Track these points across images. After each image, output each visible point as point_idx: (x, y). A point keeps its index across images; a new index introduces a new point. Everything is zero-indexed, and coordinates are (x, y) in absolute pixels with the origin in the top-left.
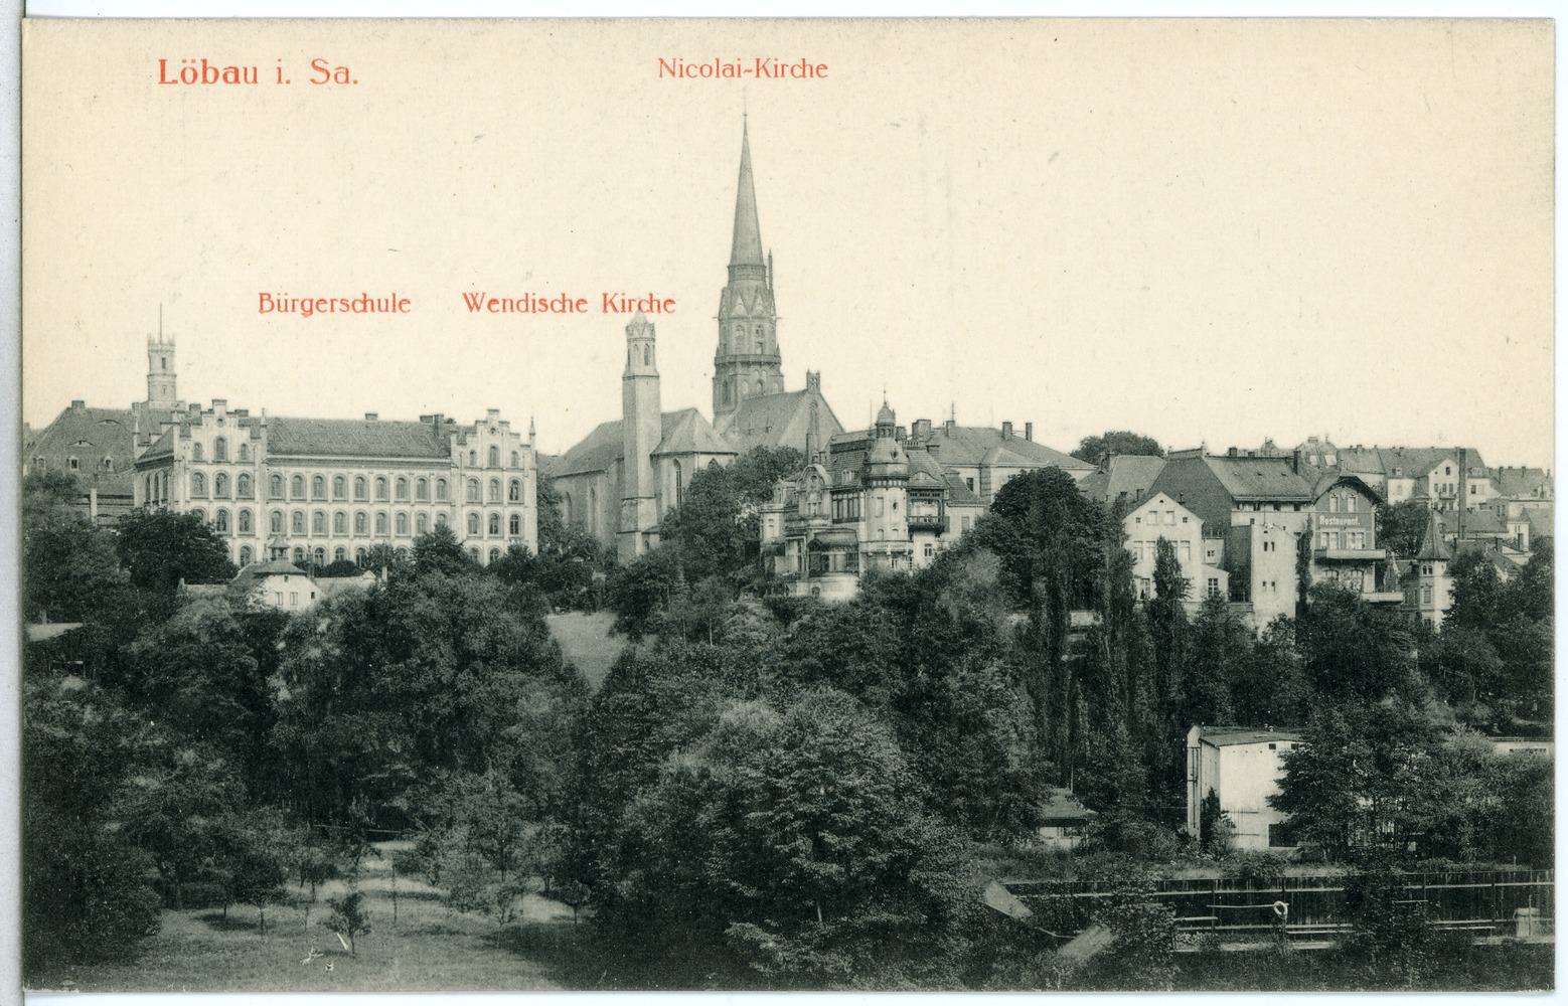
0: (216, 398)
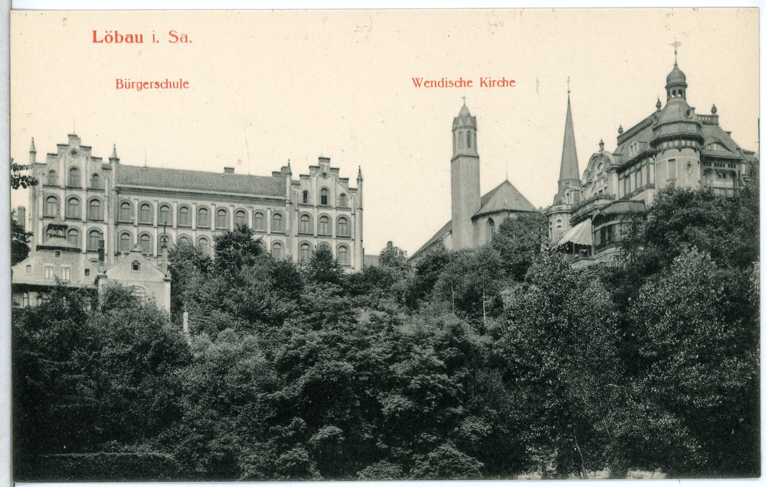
0: (302, 174)
